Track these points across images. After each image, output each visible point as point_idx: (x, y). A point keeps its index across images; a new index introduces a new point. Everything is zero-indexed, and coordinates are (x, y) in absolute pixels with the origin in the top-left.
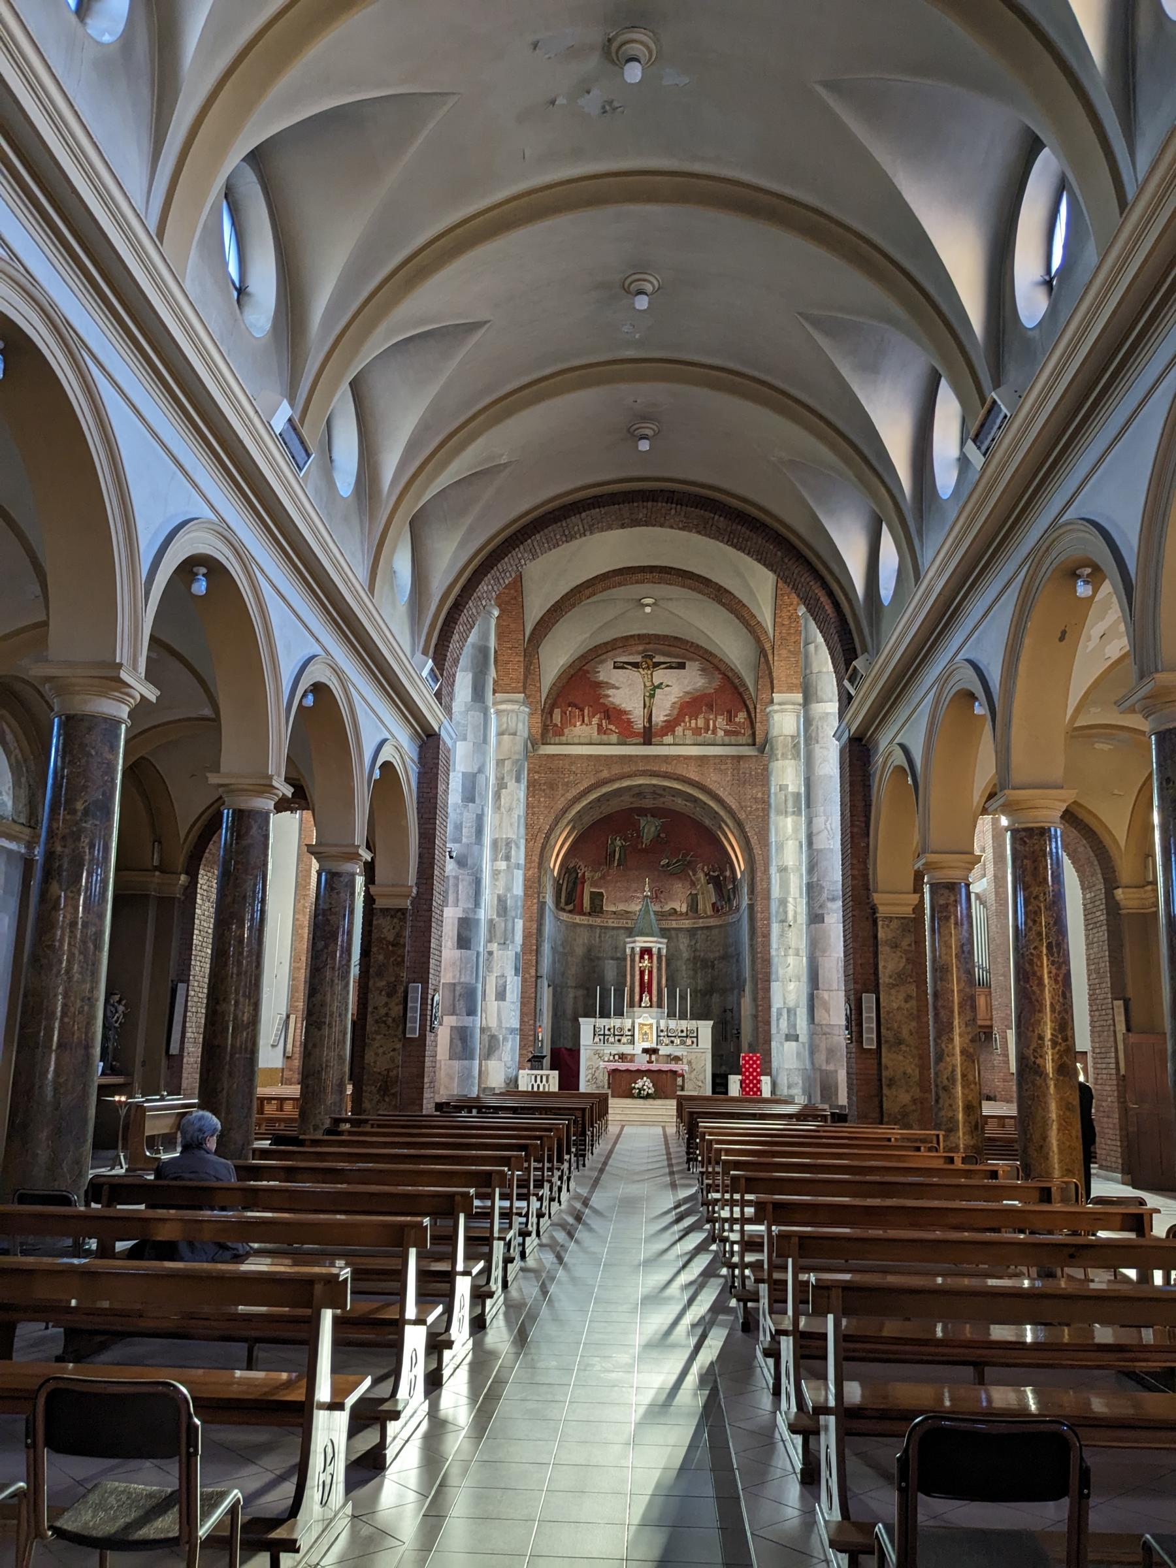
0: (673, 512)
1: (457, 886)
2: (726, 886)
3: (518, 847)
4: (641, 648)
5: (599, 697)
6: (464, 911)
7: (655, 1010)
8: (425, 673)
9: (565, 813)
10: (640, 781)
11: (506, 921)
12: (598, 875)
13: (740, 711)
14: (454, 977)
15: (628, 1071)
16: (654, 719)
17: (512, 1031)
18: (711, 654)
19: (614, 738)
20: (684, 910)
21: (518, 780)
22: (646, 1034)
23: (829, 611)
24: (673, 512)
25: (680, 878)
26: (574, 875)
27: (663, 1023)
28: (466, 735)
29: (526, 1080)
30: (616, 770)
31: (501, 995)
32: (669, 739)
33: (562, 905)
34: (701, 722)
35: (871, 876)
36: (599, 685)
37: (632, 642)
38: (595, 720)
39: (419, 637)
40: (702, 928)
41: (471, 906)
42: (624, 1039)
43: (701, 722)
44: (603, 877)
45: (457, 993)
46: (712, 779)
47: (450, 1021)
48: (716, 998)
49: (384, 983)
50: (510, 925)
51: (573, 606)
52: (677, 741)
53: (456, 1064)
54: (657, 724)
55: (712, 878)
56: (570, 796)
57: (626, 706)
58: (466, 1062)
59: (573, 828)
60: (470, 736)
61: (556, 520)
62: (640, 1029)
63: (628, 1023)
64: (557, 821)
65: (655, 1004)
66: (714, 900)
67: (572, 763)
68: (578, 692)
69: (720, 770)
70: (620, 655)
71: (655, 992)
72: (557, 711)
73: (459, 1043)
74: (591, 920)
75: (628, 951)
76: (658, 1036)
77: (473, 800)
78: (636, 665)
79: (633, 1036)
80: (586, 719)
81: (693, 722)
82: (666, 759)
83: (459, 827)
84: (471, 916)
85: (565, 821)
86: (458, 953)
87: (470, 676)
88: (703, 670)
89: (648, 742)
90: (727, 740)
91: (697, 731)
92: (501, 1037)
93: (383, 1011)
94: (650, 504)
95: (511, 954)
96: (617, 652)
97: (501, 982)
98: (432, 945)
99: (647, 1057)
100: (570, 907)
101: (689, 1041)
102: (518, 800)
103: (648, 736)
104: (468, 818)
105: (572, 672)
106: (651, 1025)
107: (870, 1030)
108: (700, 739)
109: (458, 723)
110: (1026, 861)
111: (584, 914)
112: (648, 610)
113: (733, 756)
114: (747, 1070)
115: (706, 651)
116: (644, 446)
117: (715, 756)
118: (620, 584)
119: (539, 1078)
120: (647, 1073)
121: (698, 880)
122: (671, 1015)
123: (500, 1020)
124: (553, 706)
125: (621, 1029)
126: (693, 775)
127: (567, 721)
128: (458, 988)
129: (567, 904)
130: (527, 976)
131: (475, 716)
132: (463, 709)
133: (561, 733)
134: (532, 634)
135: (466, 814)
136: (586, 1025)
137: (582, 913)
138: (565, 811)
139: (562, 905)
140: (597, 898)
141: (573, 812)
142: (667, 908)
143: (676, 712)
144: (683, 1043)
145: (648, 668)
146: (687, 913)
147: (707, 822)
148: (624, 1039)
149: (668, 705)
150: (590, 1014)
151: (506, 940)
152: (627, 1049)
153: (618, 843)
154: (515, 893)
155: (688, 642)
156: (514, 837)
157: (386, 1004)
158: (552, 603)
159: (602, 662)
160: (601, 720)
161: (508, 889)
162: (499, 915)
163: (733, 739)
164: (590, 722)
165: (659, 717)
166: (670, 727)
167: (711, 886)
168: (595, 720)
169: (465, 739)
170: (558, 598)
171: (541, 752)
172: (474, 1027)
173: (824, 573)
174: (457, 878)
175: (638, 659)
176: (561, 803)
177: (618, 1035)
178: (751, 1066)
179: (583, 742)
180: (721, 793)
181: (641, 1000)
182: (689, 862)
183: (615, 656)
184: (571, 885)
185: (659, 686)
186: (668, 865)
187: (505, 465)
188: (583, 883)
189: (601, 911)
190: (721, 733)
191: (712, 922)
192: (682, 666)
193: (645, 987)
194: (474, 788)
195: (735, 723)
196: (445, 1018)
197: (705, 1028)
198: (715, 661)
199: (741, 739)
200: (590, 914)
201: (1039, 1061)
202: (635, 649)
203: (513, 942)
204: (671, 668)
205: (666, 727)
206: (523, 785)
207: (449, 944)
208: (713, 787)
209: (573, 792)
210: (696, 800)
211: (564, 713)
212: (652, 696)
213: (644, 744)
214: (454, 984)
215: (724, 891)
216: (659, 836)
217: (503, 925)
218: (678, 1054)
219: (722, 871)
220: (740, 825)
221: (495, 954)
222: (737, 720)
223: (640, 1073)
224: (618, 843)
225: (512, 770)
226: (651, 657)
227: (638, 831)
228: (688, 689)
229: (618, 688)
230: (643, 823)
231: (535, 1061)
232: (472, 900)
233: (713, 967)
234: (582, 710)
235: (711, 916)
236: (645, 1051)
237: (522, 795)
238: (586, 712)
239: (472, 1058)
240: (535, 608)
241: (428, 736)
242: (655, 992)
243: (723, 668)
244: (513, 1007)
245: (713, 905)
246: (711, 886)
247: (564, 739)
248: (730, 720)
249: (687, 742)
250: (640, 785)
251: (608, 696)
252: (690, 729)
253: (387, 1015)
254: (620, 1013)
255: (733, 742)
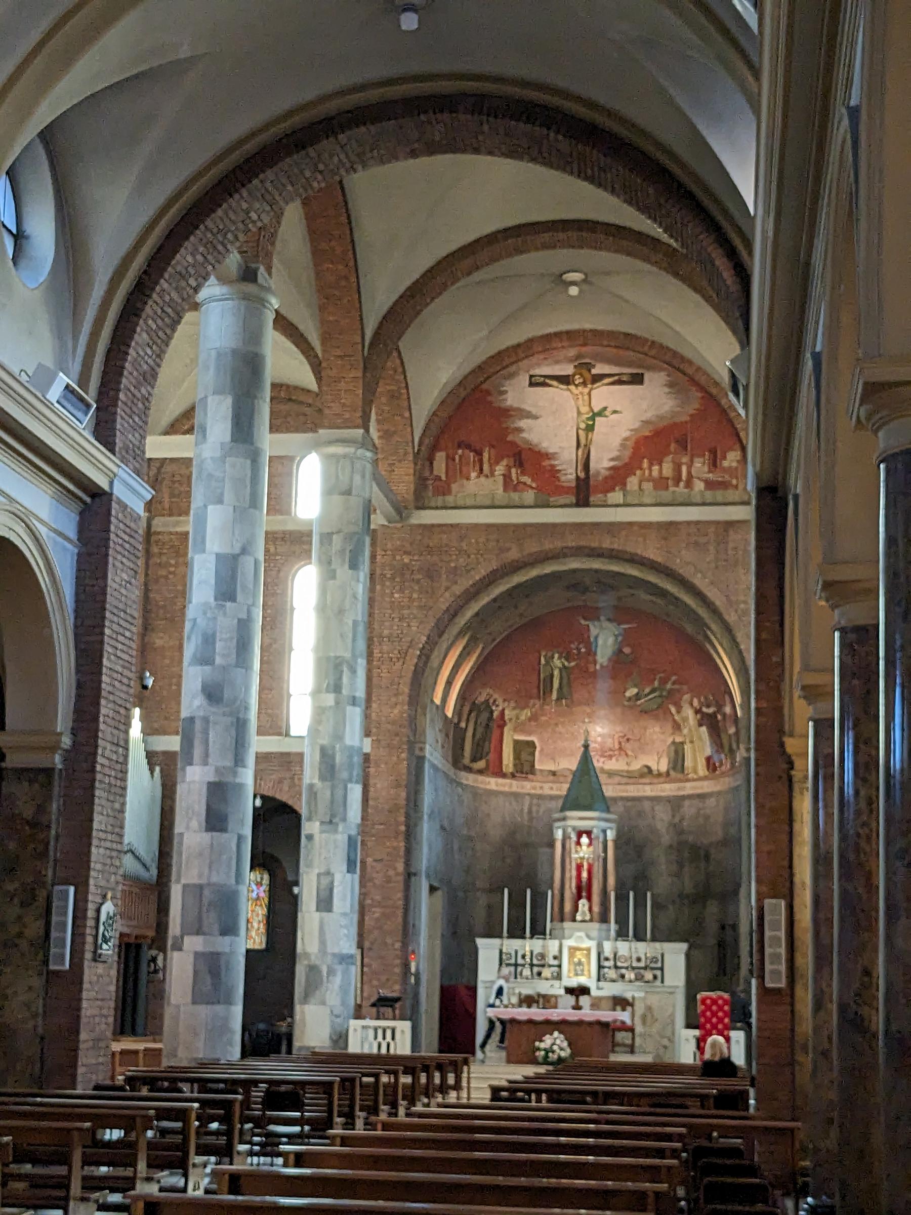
0: (486, 127)
1: (206, 732)
2: (726, 731)
3: (353, 671)
4: (572, 352)
5: (506, 431)
6: (217, 771)
7: (596, 925)
8: (55, 393)
9: (455, 615)
10: (574, 564)
11: (333, 788)
12: (526, 714)
13: (731, 449)
14: (200, 876)
15: (530, 1022)
16: (592, 465)
17: (345, 959)
18: (683, 359)
19: (529, 496)
20: (664, 766)
21: (354, 566)
22: (580, 963)
23: (729, 282)
24: (486, 127)
25: (657, 718)
26: (485, 716)
27: (608, 947)
28: (222, 494)
29: (363, 1038)
30: (532, 547)
31: (325, 903)
32: (616, 496)
33: (466, 761)
34: (667, 469)
35: (786, 711)
36: (506, 413)
37: (556, 344)
38: (500, 469)
39: (75, 338)
40: (690, 797)
41: (229, 763)
42: (546, 972)
43: (667, 469)
44: (534, 718)
45: (205, 901)
46: (684, 561)
47: (194, 944)
48: (712, 908)
49: (16, 885)
50: (339, 792)
51: (445, 287)
52: (630, 500)
53: (203, 1011)
54: (598, 473)
55: (704, 715)
56: (458, 589)
57: (548, 445)
58: (219, 1009)
59: (473, 641)
60: (228, 496)
61: (300, 146)
62: (571, 956)
63: (552, 946)
64: (440, 630)
65: (596, 916)
66: (708, 751)
67: (461, 538)
68: (475, 422)
69: (696, 544)
70: (539, 365)
71: (596, 898)
72: (440, 456)
73: (208, 980)
74: (514, 786)
75: (559, 834)
76: (600, 967)
77: (232, 598)
78: (565, 380)
79: (560, 966)
80: (486, 467)
81: (656, 468)
82: (612, 528)
83: (209, 640)
84: (229, 779)
85: (454, 630)
86: (206, 837)
87: (229, 401)
88: (671, 385)
89: (583, 502)
90: (709, 496)
91: (661, 483)
92: (324, 970)
93: (14, 929)
94: (446, 116)
95: (341, 839)
96: (534, 360)
97: (325, 881)
98: (95, 825)
99: (571, 1000)
100: (481, 764)
101: (649, 976)
102: (355, 597)
103: (584, 492)
104: (226, 625)
105: (463, 394)
106: (589, 950)
107: (776, 957)
108: (666, 496)
109: (210, 476)
110: (856, 682)
111: (504, 776)
112: (574, 291)
113: (717, 523)
114: (708, 1020)
115: (675, 354)
116: (409, 22)
117: (689, 523)
118: (519, 251)
119: (380, 1032)
120: (562, 1025)
121: (685, 719)
122: (622, 934)
123: (323, 942)
124: (434, 448)
125: (542, 956)
126: (652, 553)
127: (456, 472)
128: (206, 892)
129: (474, 759)
130: (391, 873)
131: (239, 465)
132: (218, 454)
133: (444, 490)
134: (377, 334)
135: (220, 618)
136: (488, 950)
137: (500, 774)
138: (453, 613)
139: (466, 761)
140: (525, 750)
141: (469, 613)
142: (636, 766)
143: (628, 453)
144: (640, 978)
145: (584, 384)
146: (668, 774)
147: (689, 629)
148: (546, 972)
149: (616, 442)
150: (493, 932)
151: (333, 816)
152: (544, 987)
153: (557, 662)
154: (348, 741)
155: (646, 340)
156: (347, 655)
157: (20, 918)
158: (408, 283)
159: (511, 376)
160: (509, 468)
161: (338, 736)
162: (322, 778)
163: (719, 495)
164: (492, 474)
165: (601, 462)
166: (618, 477)
167: (704, 729)
168: (500, 469)
169: (220, 501)
170: (416, 276)
171: (414, 521)
172: (232, 953)
173: (720, 218)
174: (206, 720)
175: (568, 370)
176: (444, 602)
177: (538, 964)
178: (714, 1014)
179: (481, 504)
180: (699, 581)
181: (576, 909)
182: (670, 692)
183: (533, 366)
184: (480, 730)
185: (601, 413)
186: (637, 697)
187: (192, 61)
188: (501, 727)
189: (532, 770)
190: (699, 486)
191: (707, 787)
192: (637, 379)
193: (583, 890)
194: (234, 577)
195: (724, 470)
196: (187, 939)
197: (675, 956)
198: (690, 371)
199: (732, 495)
200: (513, 776)
201: (865, 1011)
202: (562, 354)
203: (344, 819)
204: (620, 382)
205: (611, 477)
206: (363, 573)
207: (194, 824)
208: (686, 572)
209: (464, 584)
210: (663, 593)
211: (450, 458)
212: (590, 428)
213: (578, 505)
214: (201, 887)
215: (723, 736)
216: (620, 651)
217: (328, 793)
218: (628, 995)
219: (720, 707)
220: (728, 629)
221: (317, 837)
222: (726, 464)
223: (549, 1026)
224: (557, 662)
225: (342, 551)
226: (589, 367)
227: (588, 645)
228: (648, 415)
229: (536, 417)
230: (594, 631)
231: (384, 1005)
232: (230, 756)
233: (707, 857)
234: (479, 453)
235: (705, 778)
236: (570, 991)
237: (361, 589)
238: (486, 455)
239: (229, 1002)
240: (380, 293)
241: (93, 496)
242: (596, 898)
243: (703, 380)
244: (344, 921)
245: (708, 759)
246: (704, 729)
247: (450, 499)
248: (714, 464)
249: (647, 500)
250: (574, 571)
251: (520, 430)
252: (650, 479)
253: (20, 935)
254: (538, 931)
255: (720, 499)
